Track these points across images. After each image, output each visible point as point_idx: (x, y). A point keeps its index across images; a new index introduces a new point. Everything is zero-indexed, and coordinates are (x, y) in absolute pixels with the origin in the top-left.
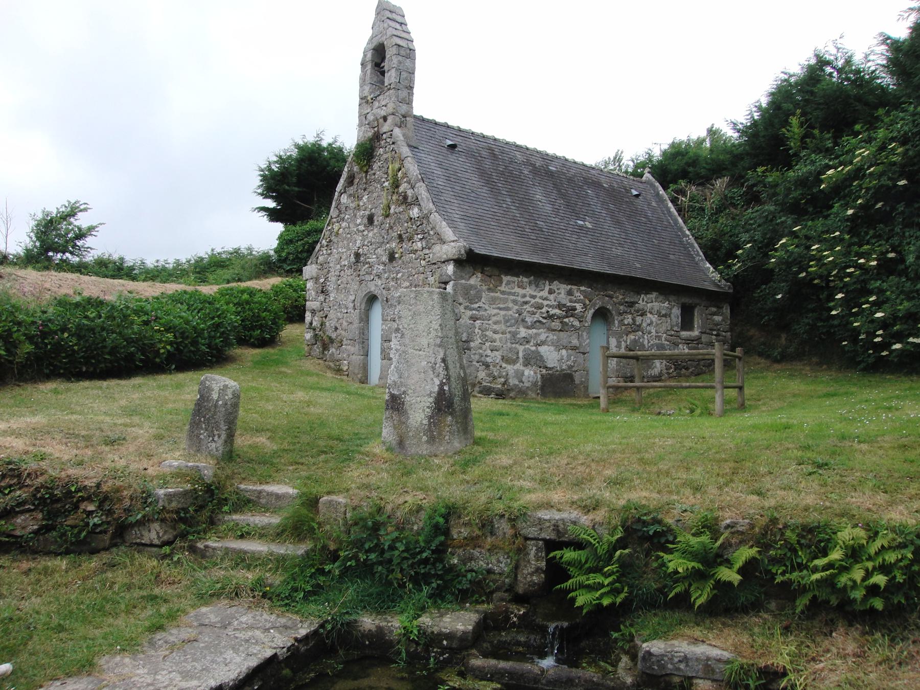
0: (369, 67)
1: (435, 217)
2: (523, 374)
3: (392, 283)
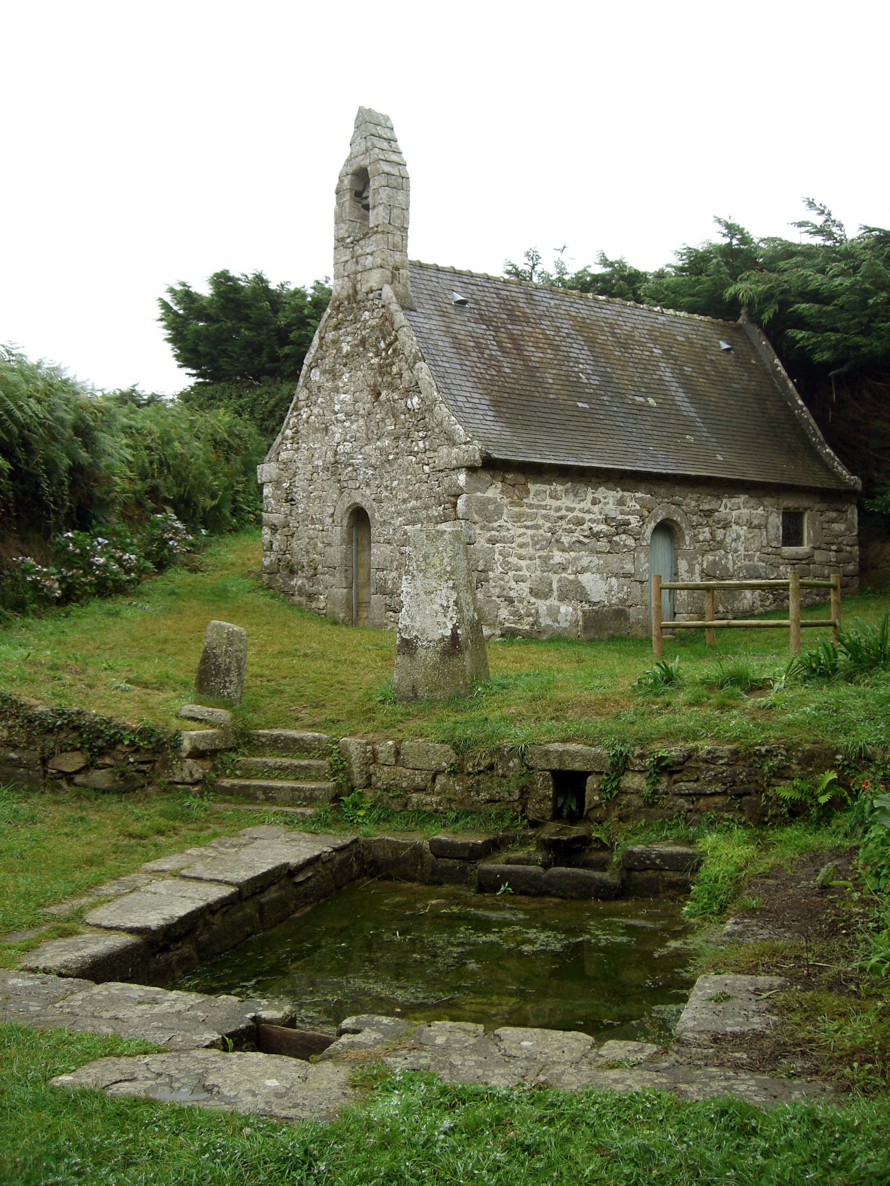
0: (347, 196)
1: (442, 410)
2: (558, 611)
3: (385, 493)
